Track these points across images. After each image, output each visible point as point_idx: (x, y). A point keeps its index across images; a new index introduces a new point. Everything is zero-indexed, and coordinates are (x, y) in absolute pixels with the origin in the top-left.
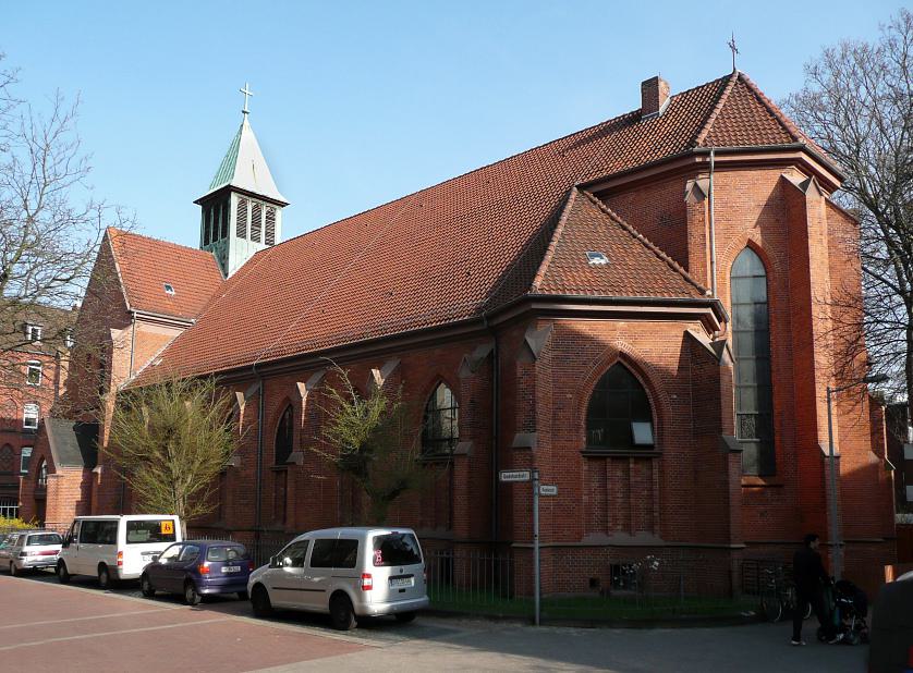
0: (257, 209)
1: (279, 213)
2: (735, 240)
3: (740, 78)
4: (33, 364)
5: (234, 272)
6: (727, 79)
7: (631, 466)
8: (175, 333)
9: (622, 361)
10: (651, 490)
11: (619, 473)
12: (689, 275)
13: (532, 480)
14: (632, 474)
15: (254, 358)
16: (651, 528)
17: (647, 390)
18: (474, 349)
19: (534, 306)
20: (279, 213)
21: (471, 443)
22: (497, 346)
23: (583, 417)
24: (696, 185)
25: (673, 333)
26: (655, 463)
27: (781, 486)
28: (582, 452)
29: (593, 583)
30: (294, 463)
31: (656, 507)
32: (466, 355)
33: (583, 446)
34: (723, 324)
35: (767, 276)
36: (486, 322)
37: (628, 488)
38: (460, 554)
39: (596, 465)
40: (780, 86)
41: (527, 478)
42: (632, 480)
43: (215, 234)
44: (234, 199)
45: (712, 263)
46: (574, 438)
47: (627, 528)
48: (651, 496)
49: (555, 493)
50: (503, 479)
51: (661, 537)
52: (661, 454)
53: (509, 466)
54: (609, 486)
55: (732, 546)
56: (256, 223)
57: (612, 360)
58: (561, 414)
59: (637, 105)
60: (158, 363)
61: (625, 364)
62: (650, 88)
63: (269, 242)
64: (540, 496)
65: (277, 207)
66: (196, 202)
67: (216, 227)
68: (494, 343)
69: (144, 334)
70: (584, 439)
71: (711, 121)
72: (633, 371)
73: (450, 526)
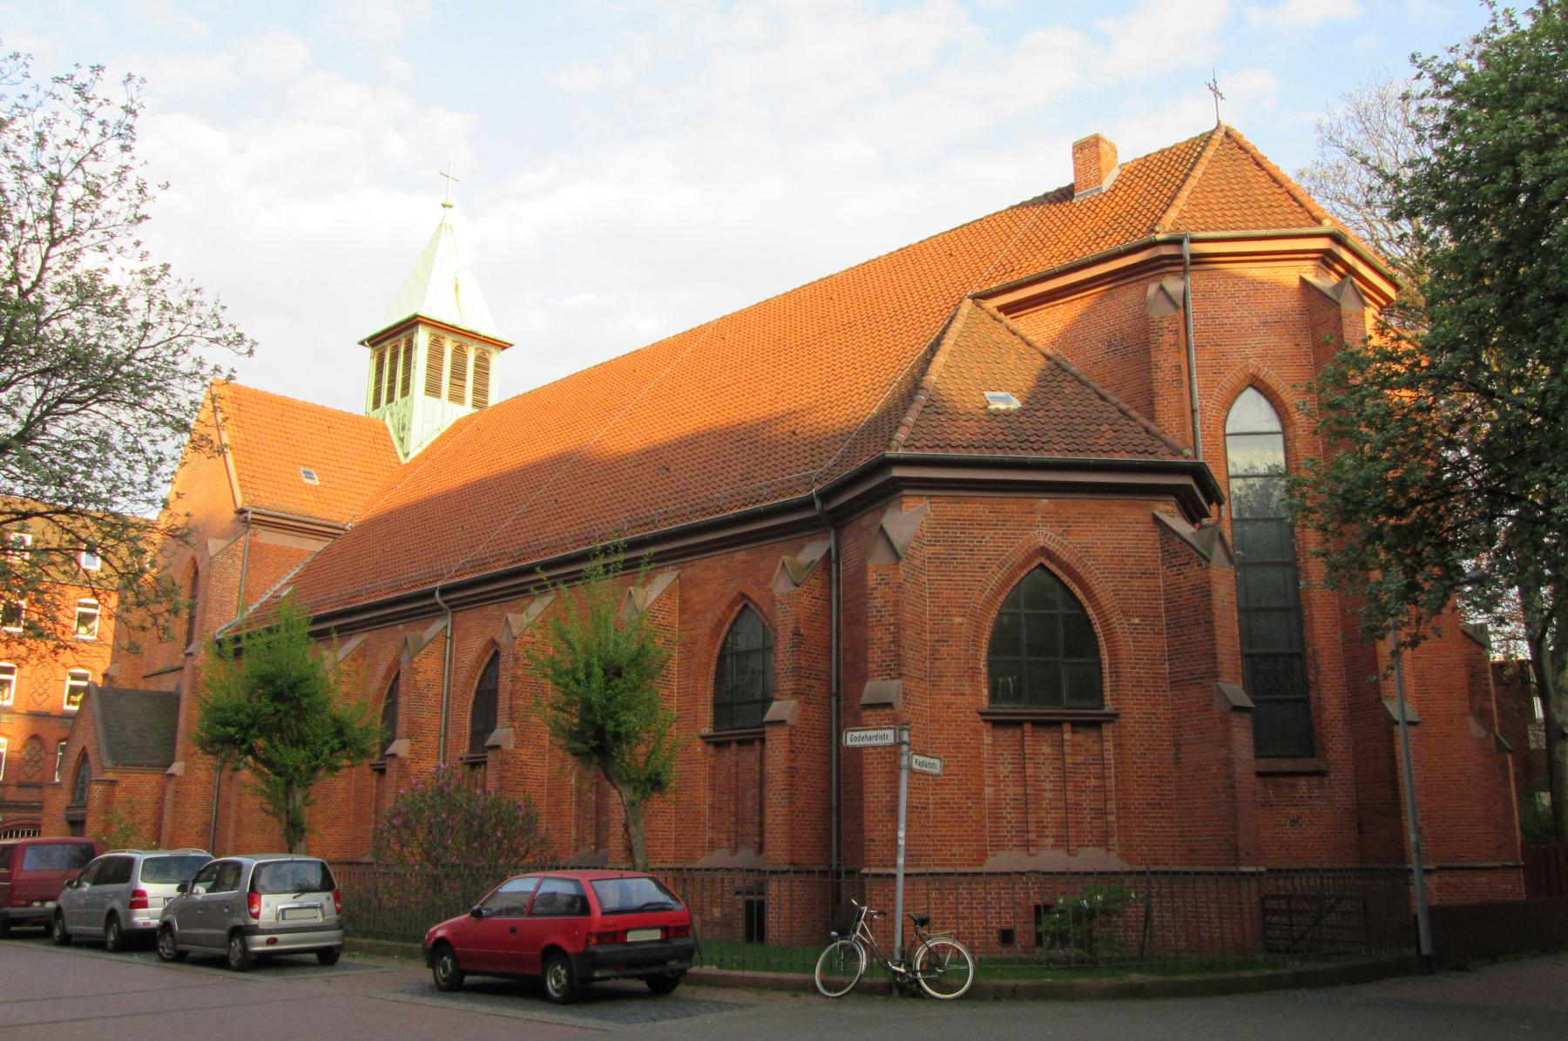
0: (459, 353)
1: (496, 359)
2: (1230, 374)
3: (1227, 135)
4: (86, 605)
5: (418, 451)
6: (1207, 138)
7: (1067, 736)
8: (316, 546)
9: (1047, 563)
10: (1102, 777)
11: (1046, 749)
12: (1153, 427)
13: (899, 743)
14: (1068, 750)
15: (440, 576)
16: (1103, 841)
17: (1090, 611)
18: (800, 549)
19: (897, 472)
20: (496, 359)
21: (793, 702)
22: (838, 543)
23: (984, 653)
24: (1162, 288)
25: (1131, 518)
26: (1107, 731)
27: (1322, 774)
28: (982, 714)
29: (1007, 936)
30: (497, 747)
31: (1112, 806)
32: (786, 558)
33: (985, 703)
34: (1214, 507)
35: (1284, 432)
36: (818, 504)
37: (1064, 774)
38: (774, 890)
39: (1008, 735)
40: (1291, 152)
41: (890, 740)
42: (1069, 759)
43: (391, 390)
44: (423, 337)
45: (1193, 411)
46: (967, 689)
47: (1062, 842)
48: (1102, 789)
49: (937, 770)
50: (849, 743)
51: (1121, 856)
52: (1116, 716)
53: (858, 724)
54: (1029, 771)
55: (1244, 869)
56: (458, 374)
57: (1028, 560)
58: (944, 650)
59: (1065, 178)
60: (284, 594)
61: (1053, 567)
62: (1088, 151)
63: (480, 402)
64: (912, 771)
65: (492, 349)
66: (362, 343)
67: (392, 380)
68: (831, 542)
69: (262, 546)
70: (985, 692)
71: (1185, 193)
72: (1065, 579)
73: (761, 848)
